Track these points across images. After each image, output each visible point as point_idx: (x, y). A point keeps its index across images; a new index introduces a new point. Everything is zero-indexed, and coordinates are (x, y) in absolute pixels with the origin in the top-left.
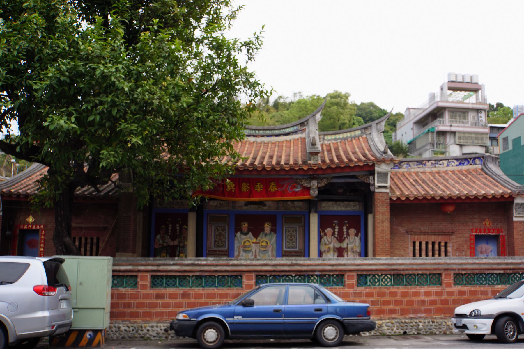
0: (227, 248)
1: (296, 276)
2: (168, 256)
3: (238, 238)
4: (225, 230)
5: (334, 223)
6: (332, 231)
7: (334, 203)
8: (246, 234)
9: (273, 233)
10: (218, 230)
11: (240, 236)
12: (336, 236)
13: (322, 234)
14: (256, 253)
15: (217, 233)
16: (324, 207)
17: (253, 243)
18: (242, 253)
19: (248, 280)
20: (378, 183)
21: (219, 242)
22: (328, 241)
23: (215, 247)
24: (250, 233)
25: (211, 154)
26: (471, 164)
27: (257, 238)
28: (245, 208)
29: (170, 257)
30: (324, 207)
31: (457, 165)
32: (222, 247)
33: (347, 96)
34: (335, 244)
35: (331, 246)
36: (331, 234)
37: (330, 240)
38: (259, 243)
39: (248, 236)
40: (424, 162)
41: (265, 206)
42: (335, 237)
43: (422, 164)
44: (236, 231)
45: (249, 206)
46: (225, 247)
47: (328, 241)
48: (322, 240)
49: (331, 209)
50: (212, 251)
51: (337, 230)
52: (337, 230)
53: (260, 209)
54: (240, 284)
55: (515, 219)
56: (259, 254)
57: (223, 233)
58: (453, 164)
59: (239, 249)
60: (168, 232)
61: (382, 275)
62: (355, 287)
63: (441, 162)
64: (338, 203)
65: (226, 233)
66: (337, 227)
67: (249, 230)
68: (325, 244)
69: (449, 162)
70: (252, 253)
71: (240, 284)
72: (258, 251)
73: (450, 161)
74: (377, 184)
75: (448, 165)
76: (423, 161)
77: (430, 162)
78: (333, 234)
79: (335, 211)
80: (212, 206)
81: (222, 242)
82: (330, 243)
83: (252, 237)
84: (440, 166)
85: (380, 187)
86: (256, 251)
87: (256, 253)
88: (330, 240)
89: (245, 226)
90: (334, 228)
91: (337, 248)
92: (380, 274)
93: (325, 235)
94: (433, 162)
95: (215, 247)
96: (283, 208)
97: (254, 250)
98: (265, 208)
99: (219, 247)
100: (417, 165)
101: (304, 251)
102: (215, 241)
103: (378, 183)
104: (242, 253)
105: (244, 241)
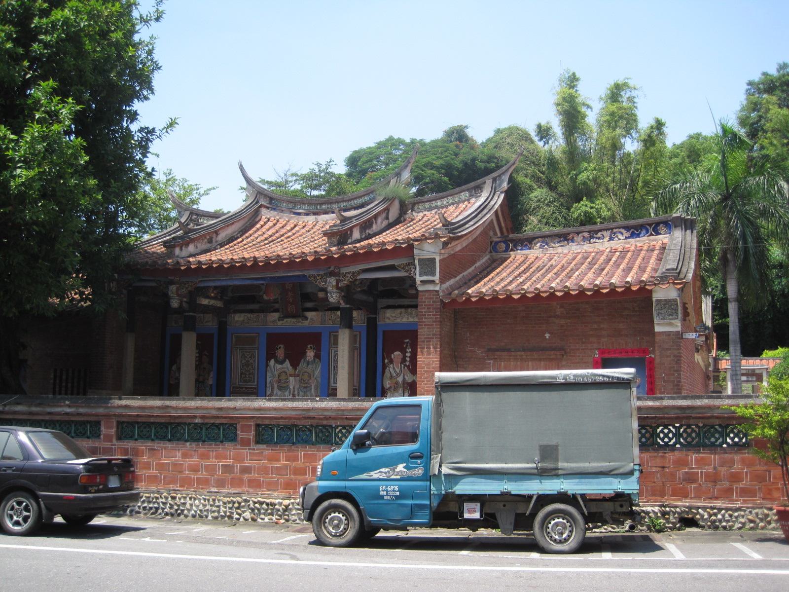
0: (256, 383)
1: (704, 426)
2: (406, 394)
3: (271, 368)
4: (254, 357)
5: (404, 343)
6: (402, 356)
7: (403, 310)
8: (282, 363)
9: (317, 360)
10: (245, 357)
11: (274, 367)
12: (408, 364)
13: (386, 361)
14: (294, 391)
15: (244, 361)
16: (388, 318)
17: (291, 375)
18: (276, 390)
19: (107, 428)
20: (420, 275)
21: (246, 375)
22: (395, 372)
23: (241, 381)
24: (287, 362)
25: (771, 245)
26: (652, 235)
27: (295, 369)
28: (280, 323)
29: (217, 395)
30: (388, 318)
31: (626, 238)
32: (250, 381)
33: (458, 135)
34: (406, 377)
35: (400, 379)
36: (400, 360)
37: (398, 371)
38: (298, 376)
39: (284, 365)
40: (571, 236)
41: (306, 318)
42: (405, 365)
43: (567, 240)
44: (268, 359)
45: (285, 320)
46: (254, 382)
47: (395, 372)
48: (387, 370)
49: (399, 320)
50: (237, 388)
51: (408, 355)
52: (408, 355)
53: (299, 325)
54: (96, 435)
55: (657, 329)
56: (298, 392)
57: (252, 361)
58: (620, 236)
59: (273, 385)
60: (405, 361)
61: (337, 427)
62: (252, 443)
63: (599, 235)
64: (409, 310)
65: (254, 361)
66: (409, 350)
67: (287, 356)
68: (391, 377)
69: (611, 232)
70: (290, 391)
71: (96, 435)
72: (296, 387)
73: (615, 230)
74: (419, 279)
75: (611, 239)
76: (569, 234)
77: (580, 235)
78: (404, 360)
79: (404, 324)
80: (237, 322)
81: (249, 374)
82: (398, 375)
83: (290, 367)
84: (597, 240)
85: (424, 282)
86: (294, 388)
87: (294, 391)
88: (398, 371)
89: (281, 352)
90: (404, 352)
91: (408, 383)
92: (701, 425)
93: (391, 362)
94: (586, 234)
95: (241, 381)
96: (330, 322)
97: (291, 387)
98: (306, 323)
99: (245, 381)
100: (559, 242)
101: (359, 385)
102: (242, 374)
103: (420, 275)
104: (276, 390)
105: (278, 372)
